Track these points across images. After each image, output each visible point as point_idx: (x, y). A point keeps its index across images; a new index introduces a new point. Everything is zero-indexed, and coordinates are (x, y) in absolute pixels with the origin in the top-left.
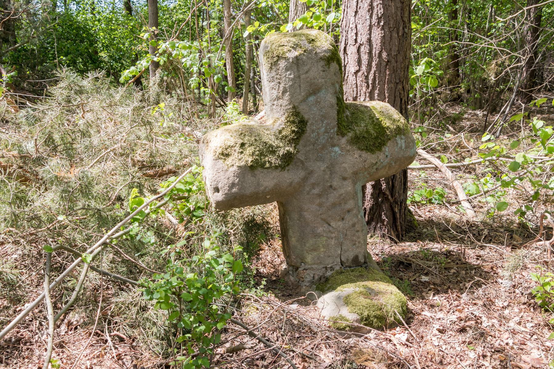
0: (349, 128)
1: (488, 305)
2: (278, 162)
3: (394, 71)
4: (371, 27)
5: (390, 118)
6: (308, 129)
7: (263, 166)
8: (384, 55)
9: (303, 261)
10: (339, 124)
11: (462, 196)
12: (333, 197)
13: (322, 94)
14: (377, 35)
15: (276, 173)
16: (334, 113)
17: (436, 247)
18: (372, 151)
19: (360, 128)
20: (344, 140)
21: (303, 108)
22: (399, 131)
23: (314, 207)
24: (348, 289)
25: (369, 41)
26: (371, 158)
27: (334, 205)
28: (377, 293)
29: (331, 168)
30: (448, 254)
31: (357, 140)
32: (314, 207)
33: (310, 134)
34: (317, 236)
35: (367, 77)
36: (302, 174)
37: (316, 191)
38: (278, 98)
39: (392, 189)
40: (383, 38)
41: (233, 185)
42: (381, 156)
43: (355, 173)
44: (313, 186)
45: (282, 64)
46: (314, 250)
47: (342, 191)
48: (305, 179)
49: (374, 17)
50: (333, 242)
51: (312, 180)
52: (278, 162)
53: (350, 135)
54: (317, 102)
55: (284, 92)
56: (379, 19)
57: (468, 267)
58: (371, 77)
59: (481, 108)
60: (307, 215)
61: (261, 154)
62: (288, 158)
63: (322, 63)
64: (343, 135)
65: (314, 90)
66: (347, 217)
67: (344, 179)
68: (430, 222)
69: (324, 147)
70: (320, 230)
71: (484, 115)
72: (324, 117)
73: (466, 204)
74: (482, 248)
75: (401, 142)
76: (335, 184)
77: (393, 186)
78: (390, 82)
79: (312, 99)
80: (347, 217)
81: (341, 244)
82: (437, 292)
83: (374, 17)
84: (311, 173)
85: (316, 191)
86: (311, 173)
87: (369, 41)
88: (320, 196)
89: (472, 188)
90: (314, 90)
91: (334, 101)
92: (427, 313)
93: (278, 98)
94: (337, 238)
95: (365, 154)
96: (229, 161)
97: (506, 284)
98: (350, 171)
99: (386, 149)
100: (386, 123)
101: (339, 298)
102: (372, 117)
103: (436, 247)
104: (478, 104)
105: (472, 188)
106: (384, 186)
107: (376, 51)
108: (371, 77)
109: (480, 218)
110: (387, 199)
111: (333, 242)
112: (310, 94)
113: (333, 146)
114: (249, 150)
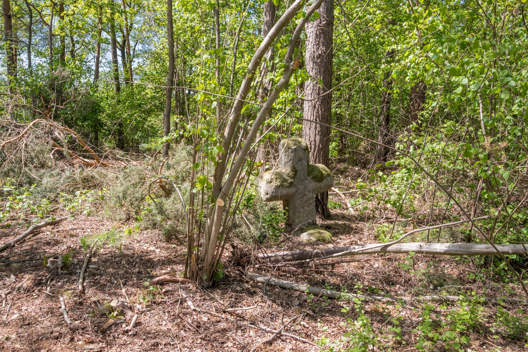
0: (311, 174)
1: (360, 239)
2: (288, 185)
3: (324, 152)
4: (315, 135)
5: (325, 170)
6: (298, 174)
7: (283, 186)
8: (321, 146)
9: (294, 222)
10: (308, 173)
11: (349, 205)
12: (305, 198)
13: (303, 161)
14: (318, 138)
15: (287, 189)
16: (306, 168)
17: (340, 222)
18: (319, 182)
19: (315, 174)
20: (309, 178)
21: (296, 166)
22: (328, 175)
23: (299, 202)
24: (311, 231)
25: (315, 140)
26: (319, 185)
27: (306, 201)
28: (322, 233)
29: (305, 188)
30: (344, 224)
31: (314, 178)
32: (299, 202)
33: (298, 175)
34: (299, 212)
35: (314, 154)
36: (295, 189)
37: (300, 196)
38: (288, 162)
39: (323, 199)
40: (320, 139)
41: (273, 192)
42: (322, 184)
43: (313, 190)
44: (299, 193)
45: (290, 150)
46: (298, 218)
47: (309, 196)
48: (296, 191)
49: (317, 131)
50: (305, 215)
51: (299, 192)
52: (288, 185)
53: (312, 176)
54: (301, 164)
55: (290, 160)
56: (319, 132)
57: (352, 229)
58: (315, 154)
59: (357, 165)
60: (297, 205)
61: (283, 182)
62: (291, 183)
63: (303, 150)
64: (309, 176)
65: (300, 160)
66: (310, 206)
67: (309, 192)
68: (336, 215)
69: (303, 180)
70: (301, 210)
71: (359, 170)
72: (303, 169)
73: (351, 209)
74: (358, 224)
75: (329, 179)
76: (306, 193)
77: (323, 197)
78: (322, 156)
79: (299, 163)
80: (310, 206)
81: (308, 216)
82: (342, 235)
83: (317, 131)
84: (298, 189)
85: (300, 196)
86: (298, 189)
87: (315, 140)
88: (301, 198)
89: (353, 203)
90: (300, 160)
91: (306, 164)
92: (339, 240)
93: (288, 162)
94: (306, 214)
95: (317, 183)
96: (272, 184)
97: (366, 234)
98: (311, 189)
99: (324, 182)
100: (324, 172)
101: (309, 234)
102: (319, 170)
103: (340, 222)
104: (355, 163)
105: (353, 203)
106: (319, 197)
107: (317, 144)
108: (315, 154)
109: (357, 213)
110: (321, 203)
111: (305, 215)
112: (299, 161)
113: (306, 180)
114: (279, 180)
